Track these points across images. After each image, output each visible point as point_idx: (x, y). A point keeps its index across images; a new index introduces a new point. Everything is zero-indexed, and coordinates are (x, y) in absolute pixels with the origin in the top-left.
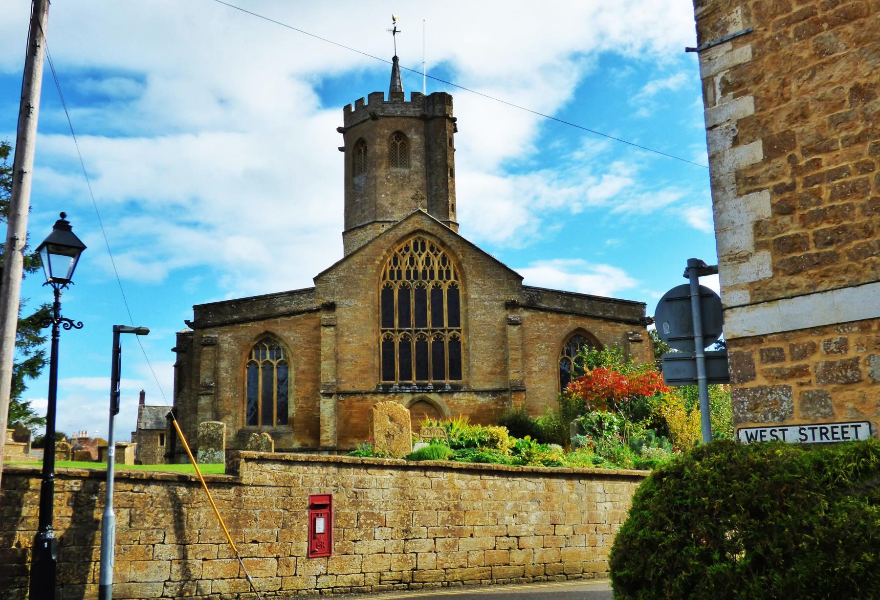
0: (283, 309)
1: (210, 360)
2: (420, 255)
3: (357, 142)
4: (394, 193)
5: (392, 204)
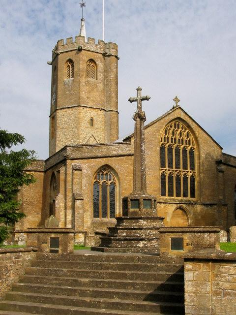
0: (115, 153)
1: (78, 179)
2: (177, 131)
3: (67, 61)
4: (89, 92)
5: (88, 98)
